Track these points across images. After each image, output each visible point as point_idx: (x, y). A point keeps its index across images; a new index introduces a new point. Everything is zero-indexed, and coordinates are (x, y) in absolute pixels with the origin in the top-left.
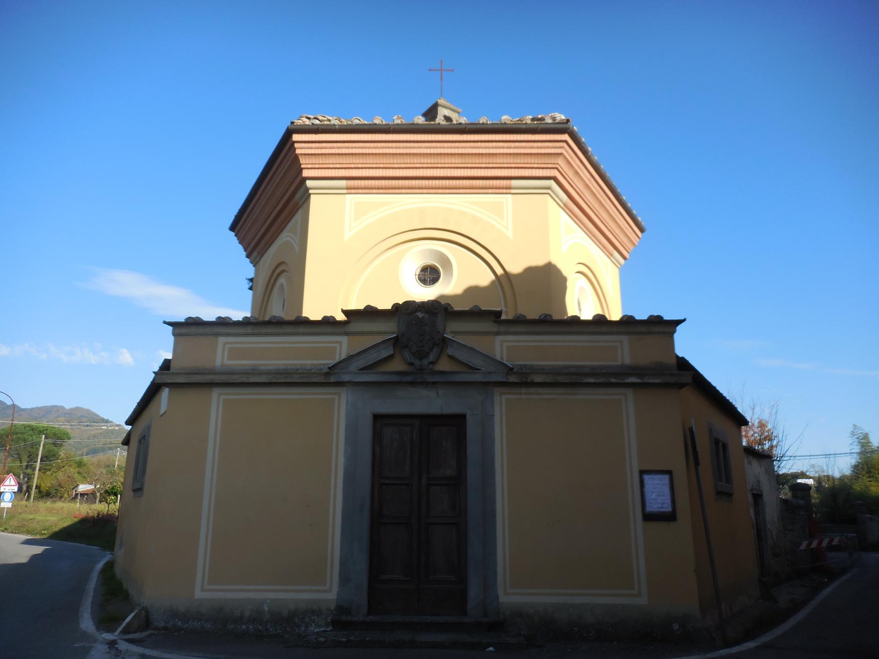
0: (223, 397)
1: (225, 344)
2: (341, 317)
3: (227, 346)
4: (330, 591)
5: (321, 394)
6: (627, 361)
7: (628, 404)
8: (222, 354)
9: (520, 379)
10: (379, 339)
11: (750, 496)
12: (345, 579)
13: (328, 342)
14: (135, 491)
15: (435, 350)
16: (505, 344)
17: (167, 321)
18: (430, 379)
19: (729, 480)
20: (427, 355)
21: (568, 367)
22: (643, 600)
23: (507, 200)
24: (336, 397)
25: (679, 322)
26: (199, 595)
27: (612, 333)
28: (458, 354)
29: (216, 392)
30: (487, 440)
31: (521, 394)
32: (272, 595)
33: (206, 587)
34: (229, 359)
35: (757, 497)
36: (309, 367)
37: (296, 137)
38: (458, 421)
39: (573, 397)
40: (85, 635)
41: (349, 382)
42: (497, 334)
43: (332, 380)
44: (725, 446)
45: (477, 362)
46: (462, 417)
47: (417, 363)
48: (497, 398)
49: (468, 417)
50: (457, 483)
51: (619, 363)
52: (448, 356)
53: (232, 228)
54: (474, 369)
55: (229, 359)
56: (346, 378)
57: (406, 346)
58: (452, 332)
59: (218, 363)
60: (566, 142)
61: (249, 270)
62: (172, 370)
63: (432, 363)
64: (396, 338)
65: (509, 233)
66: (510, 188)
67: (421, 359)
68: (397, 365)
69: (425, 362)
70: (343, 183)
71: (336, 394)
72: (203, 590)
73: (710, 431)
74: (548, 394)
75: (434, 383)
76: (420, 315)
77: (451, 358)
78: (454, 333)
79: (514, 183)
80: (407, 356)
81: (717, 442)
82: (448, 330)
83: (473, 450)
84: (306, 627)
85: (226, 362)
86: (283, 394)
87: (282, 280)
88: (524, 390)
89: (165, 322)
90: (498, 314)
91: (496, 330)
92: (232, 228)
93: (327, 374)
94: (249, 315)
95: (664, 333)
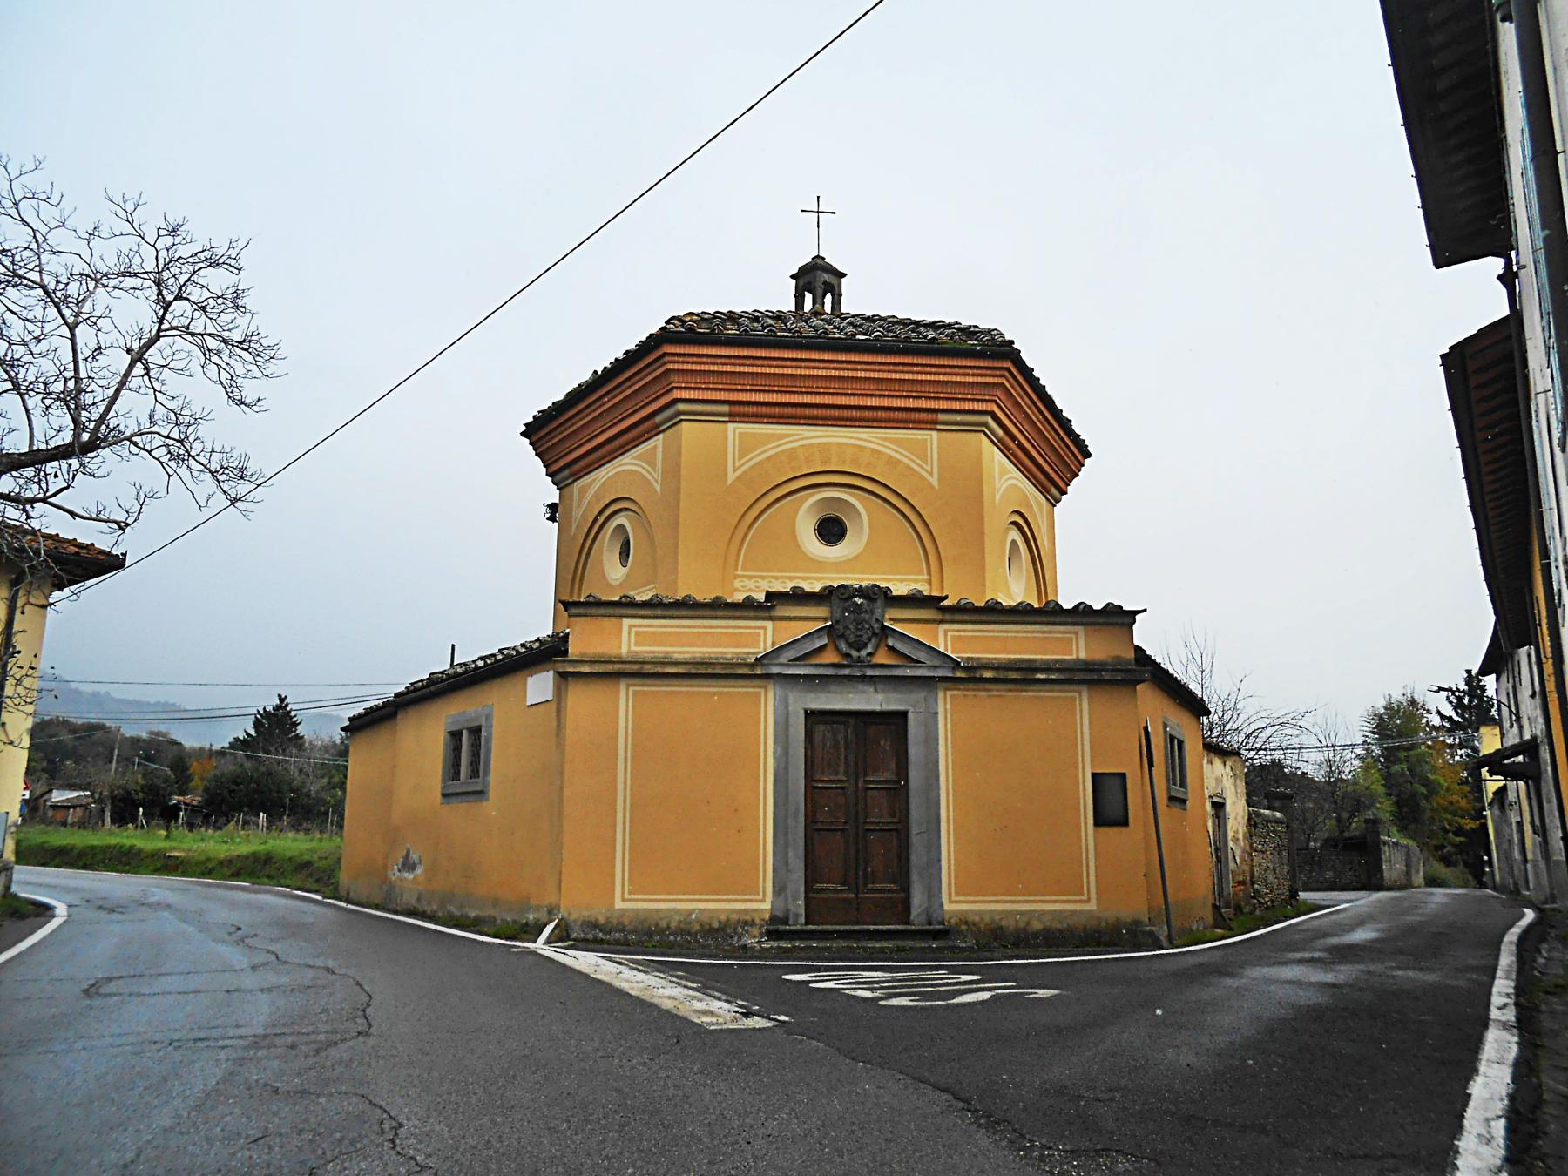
2: (761, 597)
4: (763, 900)
6: (1083, 655)
7: (1083, 707)
9: (969, 676)
11: (1208, 806)
12: (779, 889)
14: (444, 795)
18: (870, 672)
19: (1183, 784)
20: (865, 646)
22: (1092, 906)
26: (619, 905)
27: (1066, 624)
28: (898, 646)
30: (931, 740)
32: (701, 906)
34: (637, 644)
35: (1219, 807)
41: (779, 675)
42: (941, 622)
44: (1181, 743)
45: (920, 655)
46: (904, 714)
47: (854, 653)
48: (941, 694)
49: (911, 716)
50: (898, 790)
54: (916, 662)
55: (637, 644)
56: (775, 670)
60: (1008, 369)
63: (870, 654)
65: (934, 481)
67: (858, 650)
68: (830, 657)
69: (864, 653)
70: (726, 408)
72: (624, 900)
73: (1165, 726)
76: (859, 601)
77: (892, 649)
80: (844, 647)
81: (1172, 738)
83: (915, 751)
88: (970, 686)
91: (939, 617)
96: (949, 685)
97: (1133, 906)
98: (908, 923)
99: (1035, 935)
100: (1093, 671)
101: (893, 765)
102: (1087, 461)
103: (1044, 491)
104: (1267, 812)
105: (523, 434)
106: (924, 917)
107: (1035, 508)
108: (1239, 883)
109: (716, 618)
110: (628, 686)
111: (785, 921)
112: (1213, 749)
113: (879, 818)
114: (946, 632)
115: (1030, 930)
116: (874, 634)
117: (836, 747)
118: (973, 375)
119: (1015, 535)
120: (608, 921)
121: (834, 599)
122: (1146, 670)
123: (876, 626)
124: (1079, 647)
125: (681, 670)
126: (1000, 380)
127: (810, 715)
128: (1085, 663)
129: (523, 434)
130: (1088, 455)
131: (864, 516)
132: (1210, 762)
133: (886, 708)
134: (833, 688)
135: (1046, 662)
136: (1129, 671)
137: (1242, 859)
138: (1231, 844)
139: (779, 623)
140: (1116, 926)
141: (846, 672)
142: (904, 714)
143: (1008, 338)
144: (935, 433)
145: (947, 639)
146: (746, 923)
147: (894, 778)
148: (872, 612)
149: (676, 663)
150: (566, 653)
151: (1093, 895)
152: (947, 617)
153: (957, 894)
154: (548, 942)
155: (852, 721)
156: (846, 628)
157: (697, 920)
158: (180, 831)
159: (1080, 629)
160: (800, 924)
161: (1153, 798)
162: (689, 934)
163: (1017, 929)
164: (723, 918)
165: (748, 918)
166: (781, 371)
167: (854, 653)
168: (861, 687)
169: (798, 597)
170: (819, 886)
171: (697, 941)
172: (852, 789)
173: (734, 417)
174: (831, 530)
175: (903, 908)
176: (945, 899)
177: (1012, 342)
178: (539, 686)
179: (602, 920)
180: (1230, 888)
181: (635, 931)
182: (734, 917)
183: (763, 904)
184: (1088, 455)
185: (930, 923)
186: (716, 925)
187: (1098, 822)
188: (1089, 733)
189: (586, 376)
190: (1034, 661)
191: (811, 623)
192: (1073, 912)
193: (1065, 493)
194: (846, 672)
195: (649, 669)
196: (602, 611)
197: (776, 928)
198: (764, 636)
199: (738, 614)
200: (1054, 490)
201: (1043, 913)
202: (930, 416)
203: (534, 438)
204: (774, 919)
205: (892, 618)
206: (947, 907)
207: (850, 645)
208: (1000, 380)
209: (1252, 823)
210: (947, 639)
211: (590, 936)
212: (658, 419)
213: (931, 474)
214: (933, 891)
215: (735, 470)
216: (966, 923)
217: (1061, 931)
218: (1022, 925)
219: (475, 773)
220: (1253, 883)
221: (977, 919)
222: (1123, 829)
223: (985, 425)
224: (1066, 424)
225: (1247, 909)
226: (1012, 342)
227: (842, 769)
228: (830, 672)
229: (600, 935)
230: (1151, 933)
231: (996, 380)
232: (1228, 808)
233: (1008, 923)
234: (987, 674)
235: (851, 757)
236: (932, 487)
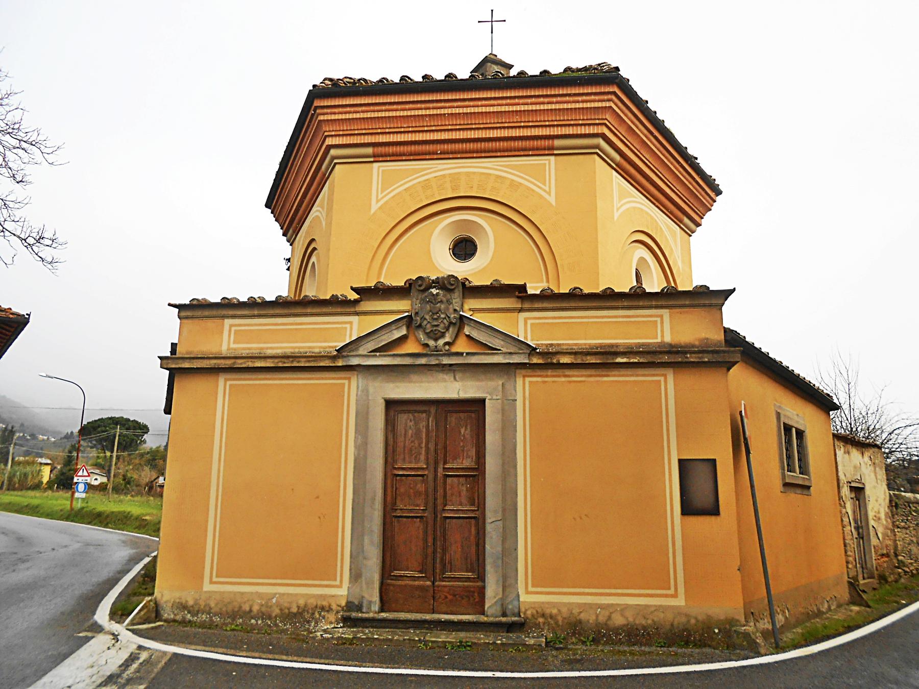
0: (229, 383)
1: (231, 326)
3: (233, 329)
4: (340, 586)
5: (333, 379)
6: (668, 339)
8: (229, 338)
9: (546, 361)
11: (845, 491)
12: (356, 576)
13: (260, 325)
15: (451, 329)
17: (172, 302)
18: (446, 361)
19: (804, 470)
20: (443, 335)
21: (601, 346)
24: (346, 382)
25: (728, 293)
26: (207, 587)
28: (475, 334)
29: (221, 379)
30: (508, 426)
31: (547, 376)
35: (858, 491)
37: (317, 103)
39: (605, 379)
40: (98, 629)
42: (521, 310)
43: (340, 364)
44: (800, 434)
46: (482, 402)
47: (431, 343)
48: (519, 381)
52: (468, 336)
53: (268, 205)
56: (355, 361)
57: (420, 326)
58: (470, 310)
60: (597, 154)
61: (286, 249)
64: (410, 317)
65: (552, 199)
66: (553, 148)
67: (436, 340)
69: (441, 342)
70: (370, 150)
71: (662, 375)
72: (211, 582)
73: (778, 415)
74: (577, 377)
75: (451, 365)
78: (474, 310)
79: (557, 143)
80: (422, 336)
81: (788, 428)
82: (466, 307)
84: (316, 623)
86: (326, 379)
87: (314, 259)
88: (549, 372)
89: (169, 305)
90: (523, 288)
92: (268, 205)
94: (285, 293)
95: (710, 306)
96: (529, 372)
97: (725, 604)
98: (483, 613)
99: (617, 631)
100: (677, 352)
101: (473, 452)
102: (718, 198)
103: (678, 221)
104: (909, 495)
106: (499, 608)
107: (667, 233)
108: (883, 555)
109: (306, 315)
110: (226, 380)
111: (359, 608)
112: (849, 440)
113: (457, 506)
114: (526, 320)
115: (610, 623)
116: (451, 323)
117: (418, 433)
118: (595, 110)
120: (196, 603)
121: (414, 292)
122: (739, 351)
124: (665, 328)
126: (608, 104)
127: (391, 404)
128: (670, 345)
130: (719, 193)
131: (491, 235)
133: (453, 395)
134: (415, 377)
135: (629, 346)
136: (717, 352)
137: (885, 535)
138: (872, 523)
140: (707, 626)
141: (423, 361)
142: (482, 402)
143: (614, 65)
144: (552, 158)
145: (529, 327)
146: (323, 608)
147: (473, 465)
148: (449, 302)
149: (266, 358)
151: (681, 590)
152: (526, 305)
153: (533, 586)
155: (433, 410)
156: (423, 318)
157: (278, 604)
158: (112, 504)
159: (665, 313)
160: (373, 610)
161: (752, 486)
162: (270, 618)
163: (598, 624)
164: (302, 602)
165: (325, 603)
166: (413, 113)
167: (431, 343)
168: (441, 376)
170: (396, 573)
171: (276, 625)
172: (431, 477)
173: (378, 158)
175: (477, 600)
176: (521, 591)
177: (617, 69)
179: (191, 603)
180: (873, 560)
181: (220, 614)
182: (312, 602)
183: (340, 591)
184: (719, 193)
185: (504, 615)
186: (295, 610)
187: (688, 509)
188: (678, 416)
190: (617, 346)
191: (384, 317)
192: (658, 608)
194: (423, 361)
195: (240, 363)
196: (207, 313)
197: (351, 616)
198: (351, 327)
199: (325, 310)
201: (627, 607)
202: (547, 143)
204: (350, 606)
205: (471, 307)
206: (523, 598)
208: (608, 104)
209: (894, 504)
210: (529, 327)
211: (179, 618)
213: (549, 193)
214: (508, 582)
215: (378, 201)
216: (543, 615)
217: (645, 628)
218: (602, 619)
220: (896, 555)
221: (555, 611)
223: (598, 147)
224: (692, 161)
225: (891, 578)
226: (617, 69)
227: (423, 457)
228: (408, 361)
229: (189, 616)
230: (746, 635)
231: (604, 104)
232: (868, 491)
233: (589, 617)
234: (565, 360)
235: (432, 446)
236: (551, 205)
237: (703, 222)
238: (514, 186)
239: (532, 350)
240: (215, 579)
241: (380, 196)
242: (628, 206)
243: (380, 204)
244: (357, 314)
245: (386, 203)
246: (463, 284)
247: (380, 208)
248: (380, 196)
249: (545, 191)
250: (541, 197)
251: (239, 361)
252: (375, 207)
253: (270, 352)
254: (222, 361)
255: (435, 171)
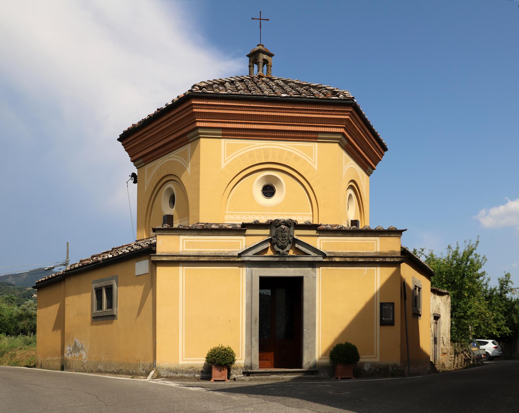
1: (183, 239)
6: (378, 250)
9: (329, 261)
10: (267, 238)
16: (322, 241)
18: (287, 259)
23: (315, 146)
33: (184, 359)
35: (437, 318)
36: (227, 253)
38: (299, 281)
42: (318, 236)
47: (281, 250)
51: (375, 251)
56: (247, 259)
59: (181, 250)
62: (157, 254)
65: (316, 167)
66: (317, 138)
67: (283, 249)
69: (285, 250)
72: (183, 360)
82: (295, 234)
85: (185, 249)
89: (406, 230)
93: (240, 255)
105: (118, 140)
107: (361, 178)
111: (251, 368)
119: (351, 191)
123: (290, 238)
125: (206, 259)
128: (380, 253)
129: (118, 140)
130: (385, 149)
131: (286, 185)
132: (435, 298)
139: (247, 237)
144: (316, 144)
145: (322, 243)
148: (289, 232)
150: (155, 252)
154: (153, 378)
169: (256, 225)
174: (269, 191)
178: (142, 267)
184: (385, 149)
189: (152, 111)
193: (374, 169)
200: (369, 168)
203: (125, 142)
204: (246, 367)
205: (297, 233)
207: (279, 247)
210: (322, 243)
212: (188, 136)
213: (314, 163)
219: (110, 305)
222: (392, 327)
234: (337, 260)
237: (377, 167)
238: (297, 158)
239: (324, 255)
240: (184, 359)
241: (226, 159)
242: (348, 167)
243: (226, 164)
244: (245, 236)
245: (230, 163)
246: (295, 223)
247: (226, 166)
248: (226, 159)
249: (312, 162)
250: (310, 165)
251: (192, 258)
252: (223, 165)
253: (204, 253)
254: (183, 258)
255: (255, 146)
